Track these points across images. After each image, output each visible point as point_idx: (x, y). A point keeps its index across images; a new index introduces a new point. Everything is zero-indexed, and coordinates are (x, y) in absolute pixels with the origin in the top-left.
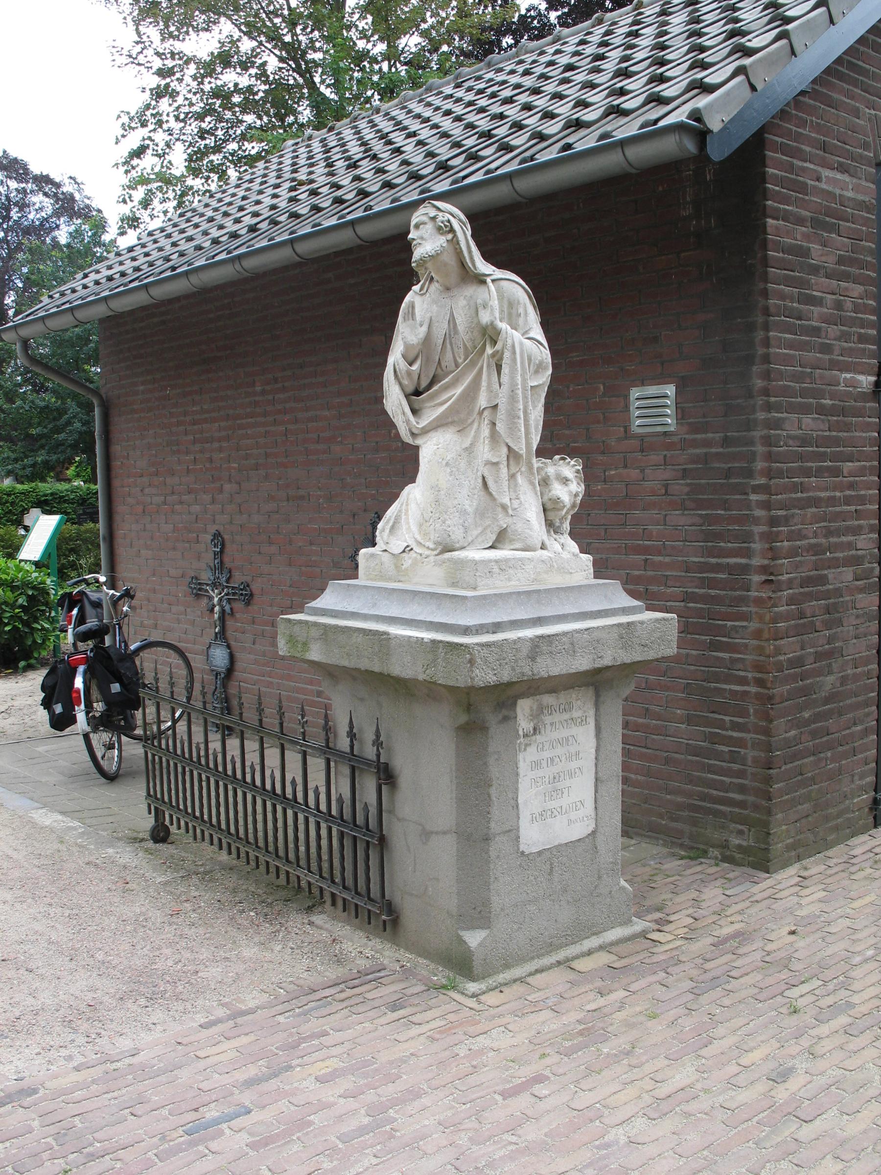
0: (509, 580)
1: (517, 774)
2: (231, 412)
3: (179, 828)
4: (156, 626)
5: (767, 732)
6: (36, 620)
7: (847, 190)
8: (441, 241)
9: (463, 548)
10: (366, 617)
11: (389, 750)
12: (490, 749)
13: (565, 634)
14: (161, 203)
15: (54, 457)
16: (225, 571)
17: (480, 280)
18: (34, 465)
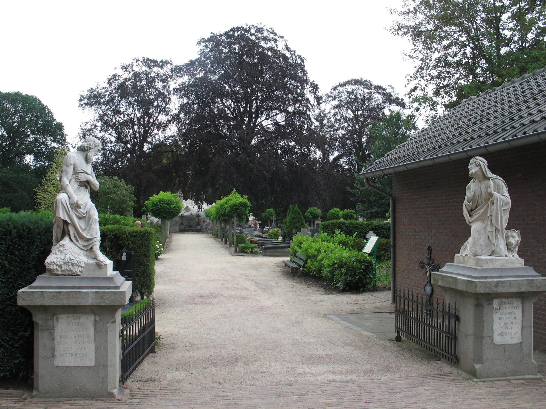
0: (493, 265)
1: (493, 321)
3: (404, 337)
4: (408, 278)
6: (368, 274)
8: (477, 168)
9: (481, 255)
10: (453, 274)
13: (507, 281)
14: (424, 108)
15: (380, 210)
17: (489, 179)
18: (372, 213)
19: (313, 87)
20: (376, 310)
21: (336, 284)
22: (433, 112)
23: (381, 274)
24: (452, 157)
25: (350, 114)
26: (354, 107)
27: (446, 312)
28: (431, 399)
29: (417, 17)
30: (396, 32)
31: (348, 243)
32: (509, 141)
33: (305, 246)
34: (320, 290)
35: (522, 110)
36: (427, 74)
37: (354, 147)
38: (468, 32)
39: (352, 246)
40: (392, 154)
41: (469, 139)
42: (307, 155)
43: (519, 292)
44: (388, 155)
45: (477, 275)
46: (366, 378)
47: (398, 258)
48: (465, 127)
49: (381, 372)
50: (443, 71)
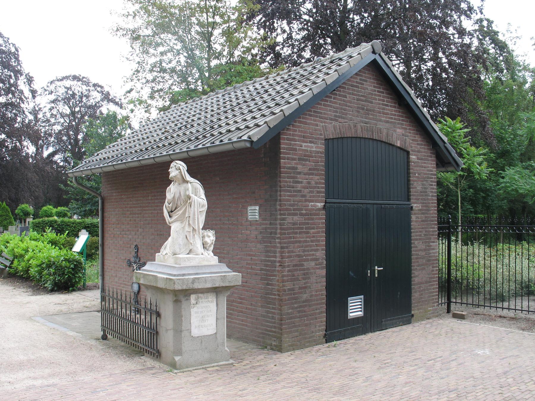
2: (141, 205)
4: (116, 276)
5: (280, 310)
6: (77, 273)
7: (313, 148)
9: (179, 254)
10: (154, 272)
11: (159, 308)
12: (182, 307)
13: (203, 277)
16: (138, 258)
17: (187, 182)
18: (85, 211)
19: (27, 79)
20: (85, 309)
21: (44, 284)
22: (147, 115)
23: (92, 272)
24: (157, 160)
25: (67, 111)
26: (71, 103)
27: (148, 309)
28: (133, 394)
29: (136, 21)
30: (115, 33)
31: (59, 242)
32: (207, 148)
33: (11, 245)
34: (27, 292)
35: (221, 120)
36: (143, 77)
37: (70, 144)
38: (183, 41)
39: (63, 245)
40: (102, 154)
41: (173, 143)
42: (19, 150)
43: (214, 287)
44: (98, 155)
45: (175, 273)
46: (69, 380)
47: (107, 257)
48: (171, 131)
49: (85, 372)
50: (158, 76)
